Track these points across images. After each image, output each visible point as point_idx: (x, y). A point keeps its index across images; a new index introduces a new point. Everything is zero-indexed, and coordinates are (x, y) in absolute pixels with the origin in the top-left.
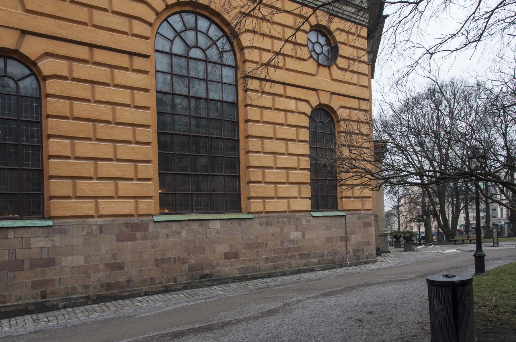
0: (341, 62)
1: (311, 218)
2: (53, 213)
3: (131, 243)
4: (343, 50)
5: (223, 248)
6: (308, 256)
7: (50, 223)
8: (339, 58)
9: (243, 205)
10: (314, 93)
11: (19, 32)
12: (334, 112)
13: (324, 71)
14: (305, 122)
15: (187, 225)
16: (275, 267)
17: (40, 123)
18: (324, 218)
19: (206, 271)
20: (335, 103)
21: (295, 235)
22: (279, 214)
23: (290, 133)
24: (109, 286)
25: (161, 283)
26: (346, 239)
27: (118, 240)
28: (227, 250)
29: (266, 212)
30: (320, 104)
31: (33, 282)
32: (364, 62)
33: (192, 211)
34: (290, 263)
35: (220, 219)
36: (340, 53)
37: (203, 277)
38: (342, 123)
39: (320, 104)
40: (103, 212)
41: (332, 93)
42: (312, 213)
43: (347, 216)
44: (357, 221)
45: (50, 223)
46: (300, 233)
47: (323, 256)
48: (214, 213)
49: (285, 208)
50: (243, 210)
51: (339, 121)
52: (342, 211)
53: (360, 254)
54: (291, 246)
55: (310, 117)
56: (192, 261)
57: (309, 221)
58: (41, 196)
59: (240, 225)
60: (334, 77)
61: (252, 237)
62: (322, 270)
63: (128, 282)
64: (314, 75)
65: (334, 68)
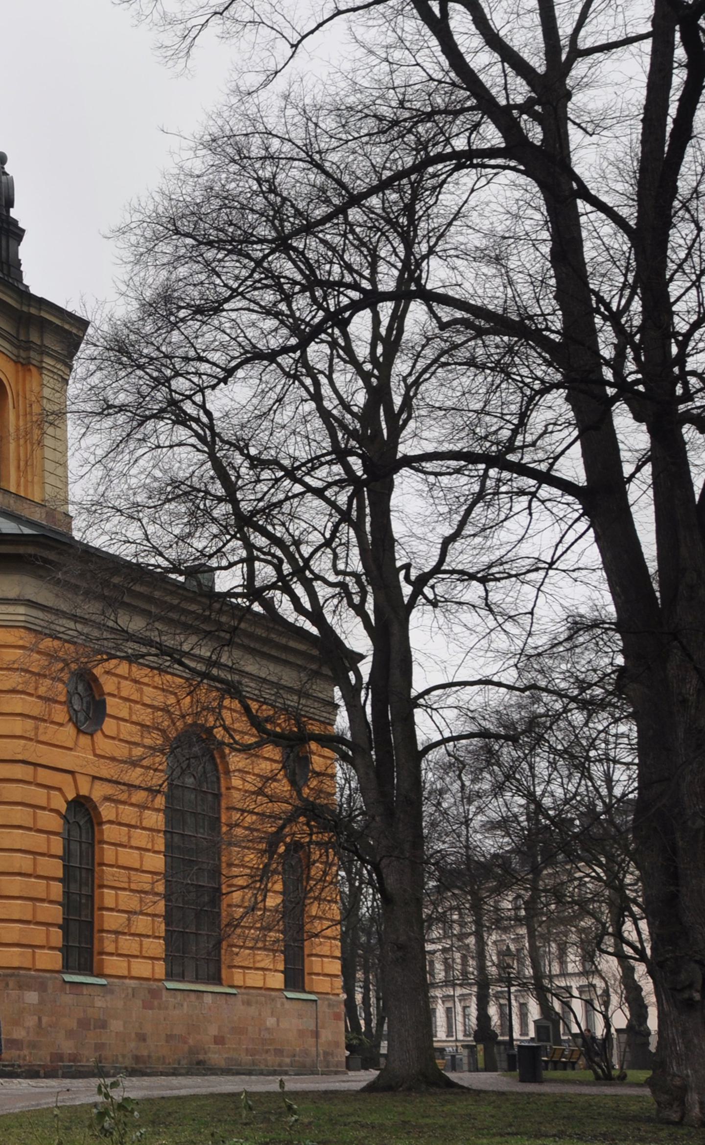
0: (109, 726)
1: (285, 1000)
2: (107, 971)
3: (150, 1011)
4: (112, 705)
5: (213, 1031)
6: (279, 1052)
7: (103, 981)
8: (107, 719)
9: (224, 976)
10: (69, 777)
11: (89, 779)
12: (95, 808)
13: (84, 740)
14: (55, 823)
15: (188, 996)
16: (254, 1063)
17: (92, 871)
18: (297, 1002)
19: (201, 1057)
20: (98, 792)
21: (271, 1022)
22: (9, 971)
23: (38, 841)
24: (137, 1058)
25: (169, 1064)
26: (316, 1035)
27: (144, 1007)
28: (216, 1034)
29: (247, 988)
30: (78, 796)
31: (96, 1044)
32: (60, 703)
33: (183, 978)
34: (266, 1060)
35: (212, 992)
36: (109, 711)
37: (199, 1063)
38: (106, 827)
39: (78, 796)
40: (134, 973)
41: (95, 778)
42: (285, 993)
43: (319, 1002)
44: (327, 1010)
45: (103, 981)
46: (275, 1019)
47: (294, 1056)
48: (201, 983)
49: (260, 984)
50: (224, 982)
51: (101, 823)
52: (310, 993)
53: (330, 1058)
54: (267, 1036)
55: (64, 817)
56: (191, 1042)
57: (283, 1004)
58: (90, 951)
59: (198, 998)
60: (98, 752)
61: (236, 1018)
62: (295, 1075)
63: (149, 1057)
64: (70, 749)
65: (98, 736)
